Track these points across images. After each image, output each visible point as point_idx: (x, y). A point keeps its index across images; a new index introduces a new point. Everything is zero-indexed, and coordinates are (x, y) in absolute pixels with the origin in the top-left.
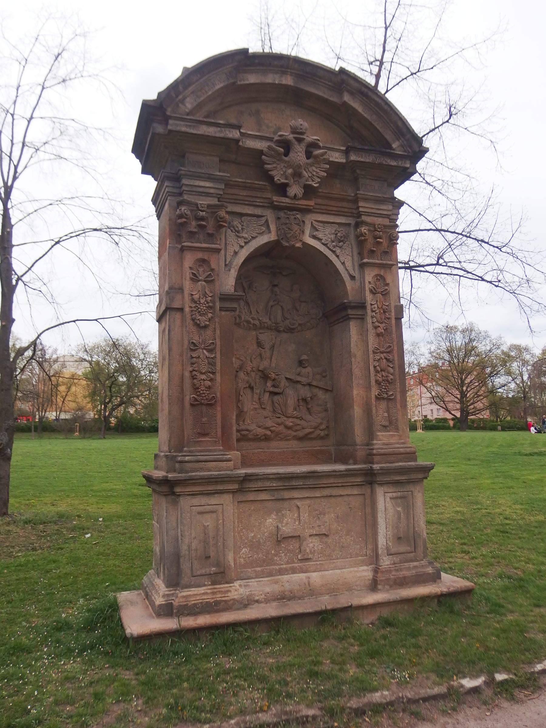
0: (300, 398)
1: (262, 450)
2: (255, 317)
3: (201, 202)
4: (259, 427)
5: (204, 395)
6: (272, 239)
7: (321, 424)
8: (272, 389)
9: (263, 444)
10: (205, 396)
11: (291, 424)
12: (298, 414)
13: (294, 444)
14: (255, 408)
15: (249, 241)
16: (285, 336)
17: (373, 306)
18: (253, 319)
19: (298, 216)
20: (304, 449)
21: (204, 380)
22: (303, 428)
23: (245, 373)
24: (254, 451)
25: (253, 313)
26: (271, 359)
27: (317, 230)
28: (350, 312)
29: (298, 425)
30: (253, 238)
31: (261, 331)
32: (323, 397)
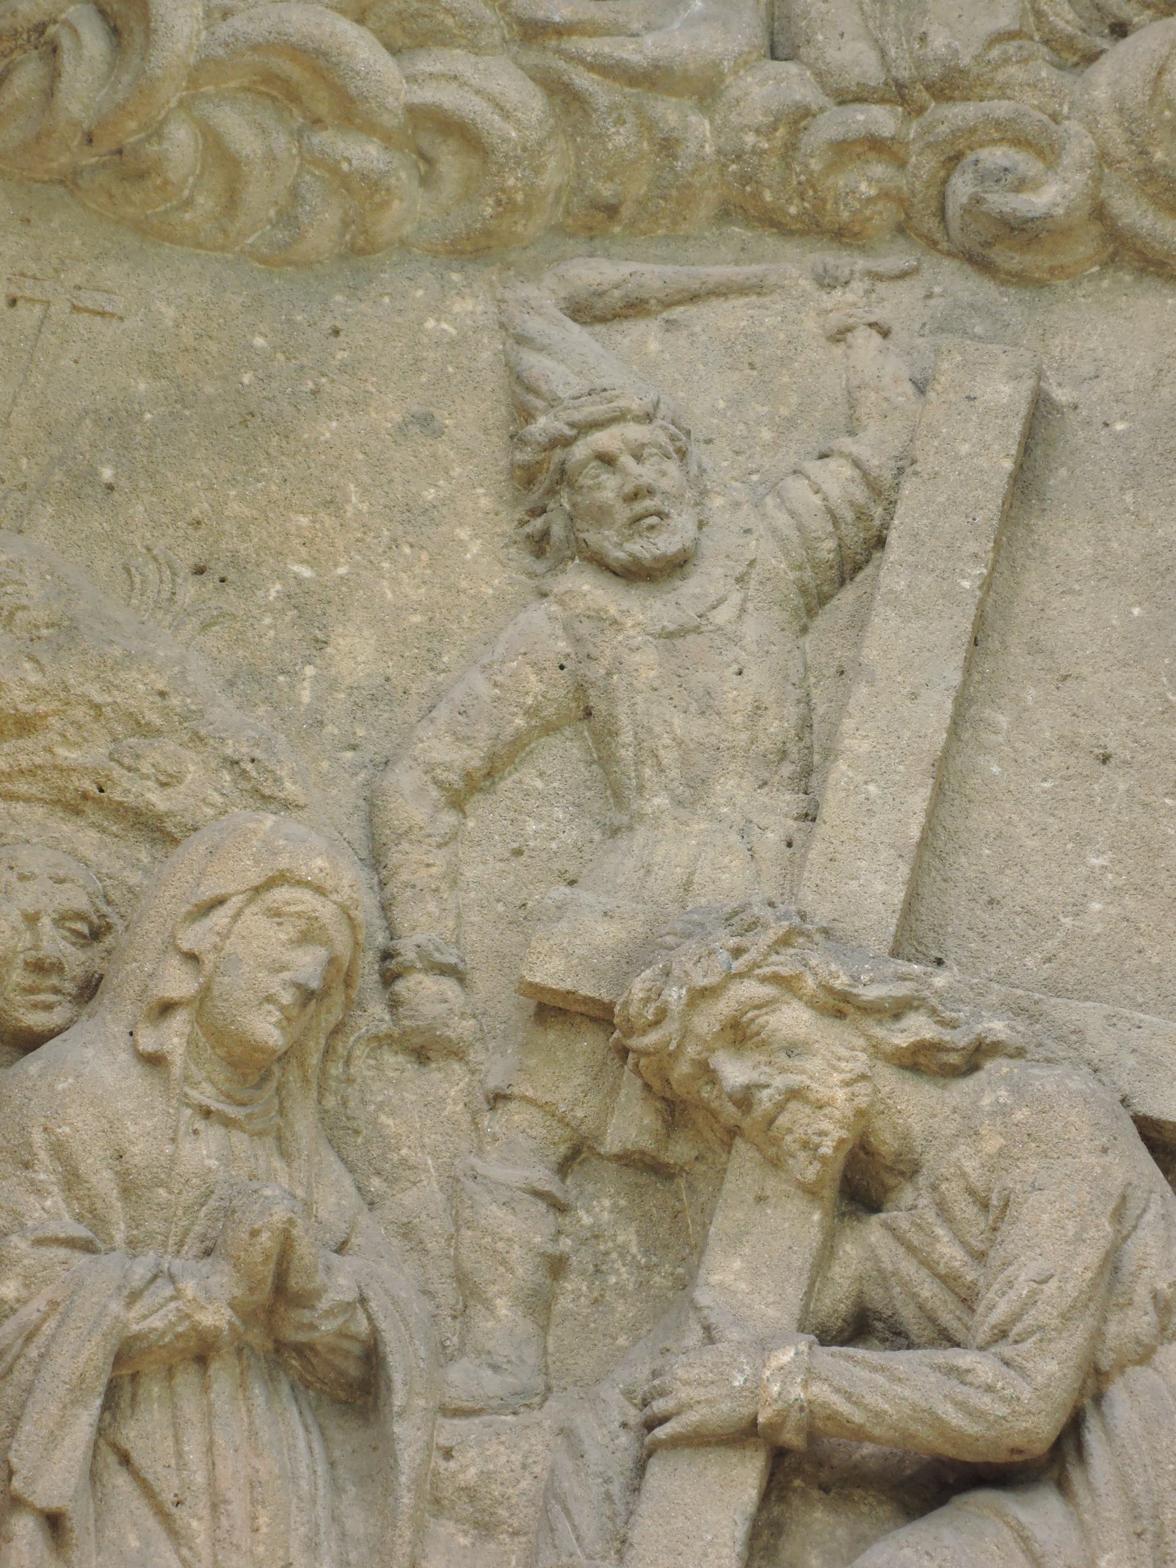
8: (793, 1378)
26: (803, 765)
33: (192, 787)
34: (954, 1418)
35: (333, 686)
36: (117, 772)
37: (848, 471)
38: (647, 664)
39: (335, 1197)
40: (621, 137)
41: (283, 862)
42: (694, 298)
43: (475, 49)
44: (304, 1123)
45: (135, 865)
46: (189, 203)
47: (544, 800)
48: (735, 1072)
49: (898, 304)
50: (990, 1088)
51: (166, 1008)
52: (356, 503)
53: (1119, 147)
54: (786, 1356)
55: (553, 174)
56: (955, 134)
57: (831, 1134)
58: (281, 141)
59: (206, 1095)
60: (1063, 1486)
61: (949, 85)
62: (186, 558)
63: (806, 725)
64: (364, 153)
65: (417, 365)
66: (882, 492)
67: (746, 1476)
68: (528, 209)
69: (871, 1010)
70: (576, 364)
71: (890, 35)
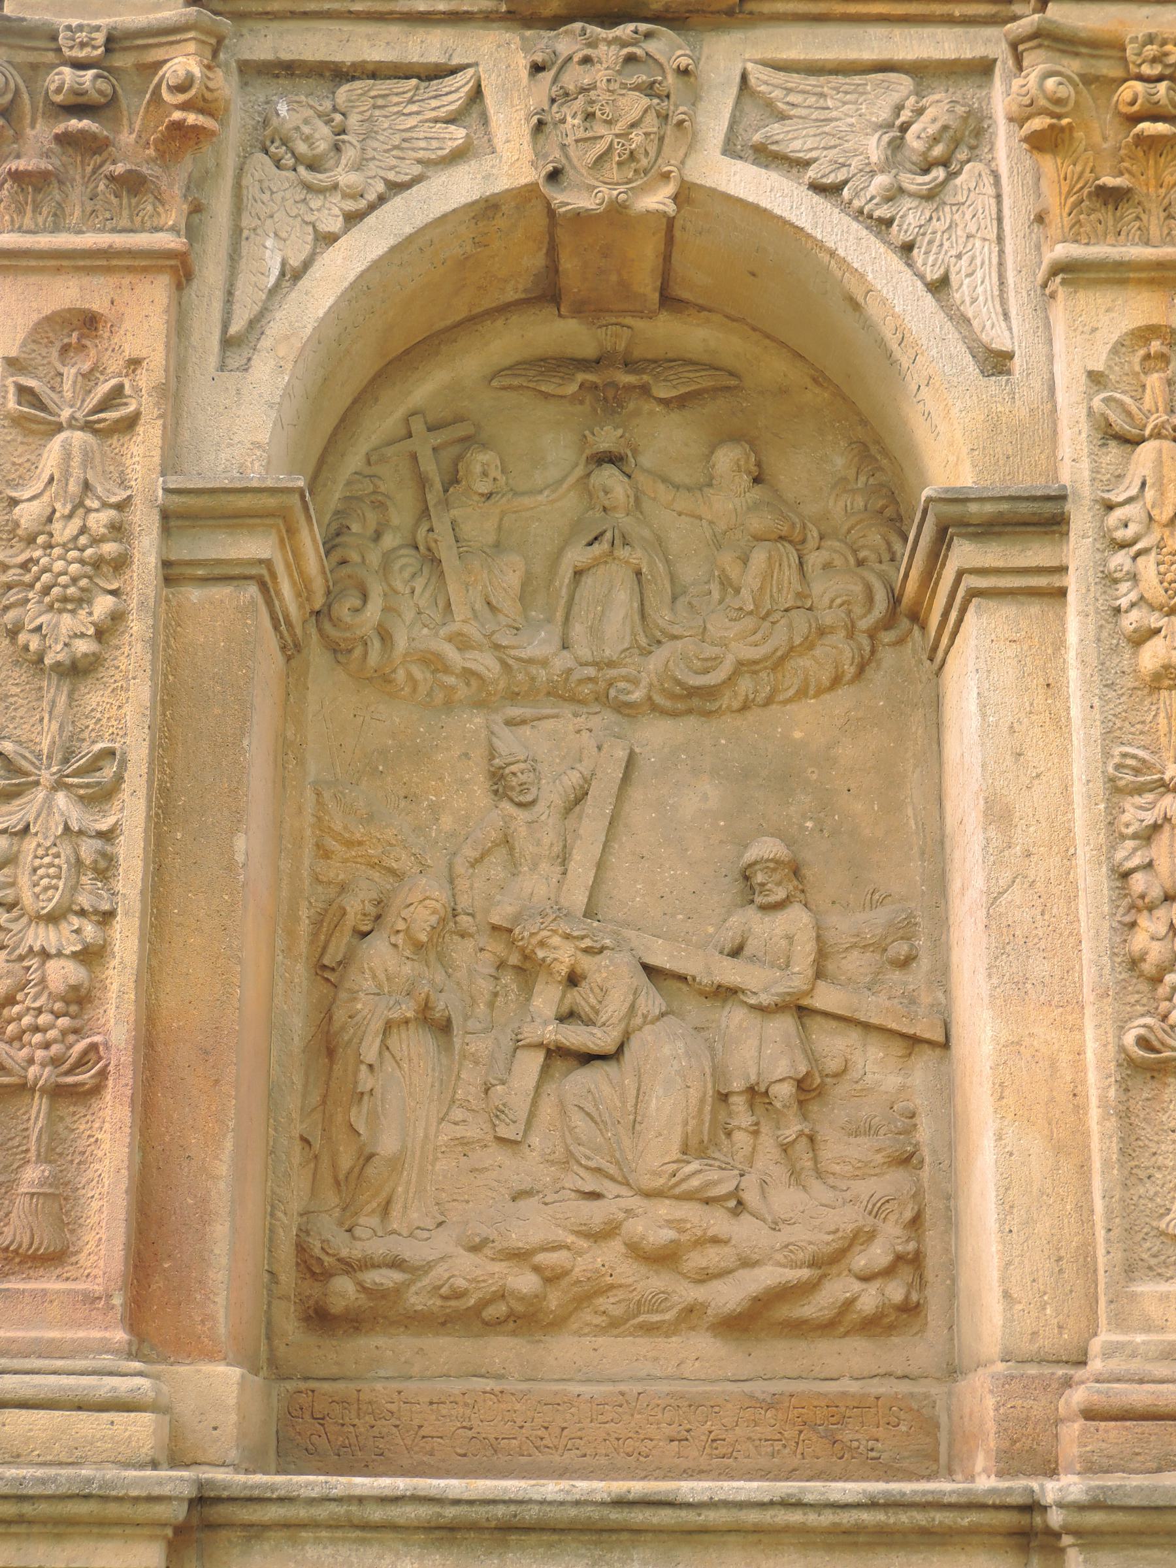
0: (737, 1085)
1: (489, 1385)
2: (472, 631)
3: (75, 22)
4: (475, 1249)
5: (38, 1038)
6: (502, 184)
7: (861, 1237)
8: (552, 1033)
9: (502, 1350)
10: (47, 1046)
11: (668, 1234)
12: (715, 1175)
13: (701, 1356)
14: (463, 1142)
15: (372, 207)
16: (656, 736)
17: (1118, 513)
18: (462, 643)
19: (652, 46)
20: (758, 1388)
21: (45, 955)
22: (747, 1263)
23: (400, 940)
24: (441, 1385)
25: (460, 611)
26: (564, 859)
27: (782, 117)
28: (964, 553)
29: (716, 1241)
30: (397, 187)
31: (514, 712)
32: (892, 1082)
33: (404, 862)
34: (592, 1046)
35: (441, 832)
36: (384, 858)
37: (578, 775)
38: (523, 831)
39: (440, 977)
40: (520, 677)
41: (428, 894)
42: (539, 719)
43: (481, 651)
44: (432, 957)
45: (389, 883)
46: (403, 689)
47: (495, 867)
48: (541, 954)
49: (595, 722)
50: (603, 960)
51: (398, 932)
52: (447, 779)
53: (655, 682)
54: (551, 1028)
55: (502, 685)
56: (611, 678)
57: (564, 970)
58: (429, 675)
59: (407, 953)
60: (618, 1060)
61: (611, 664)
62: (402, 793)
63: (565, 846)
64: (451, 680)
65: (464, 738)
66: (587, 781)
67: (539, 1057)
68: (495, 694)
69: (576, 938)
70: (509, 743)
71: (594, 648)
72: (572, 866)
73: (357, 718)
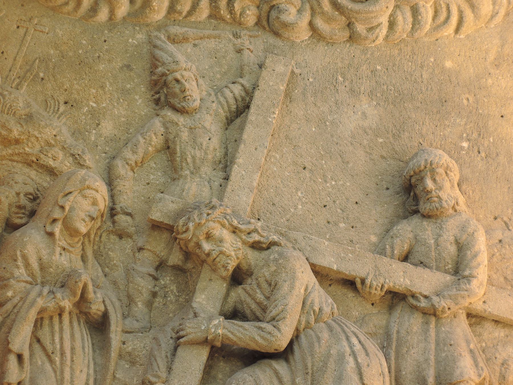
8: (222, 329)
36: (42, 156)
37: (240, 87)
45: (46, 181)
52: (108, 87)
57: (232, 266)
63: (226, 154)
65: (126, 51)
67: (204, 353)
72: (236, 171)
73: (21, 29)
